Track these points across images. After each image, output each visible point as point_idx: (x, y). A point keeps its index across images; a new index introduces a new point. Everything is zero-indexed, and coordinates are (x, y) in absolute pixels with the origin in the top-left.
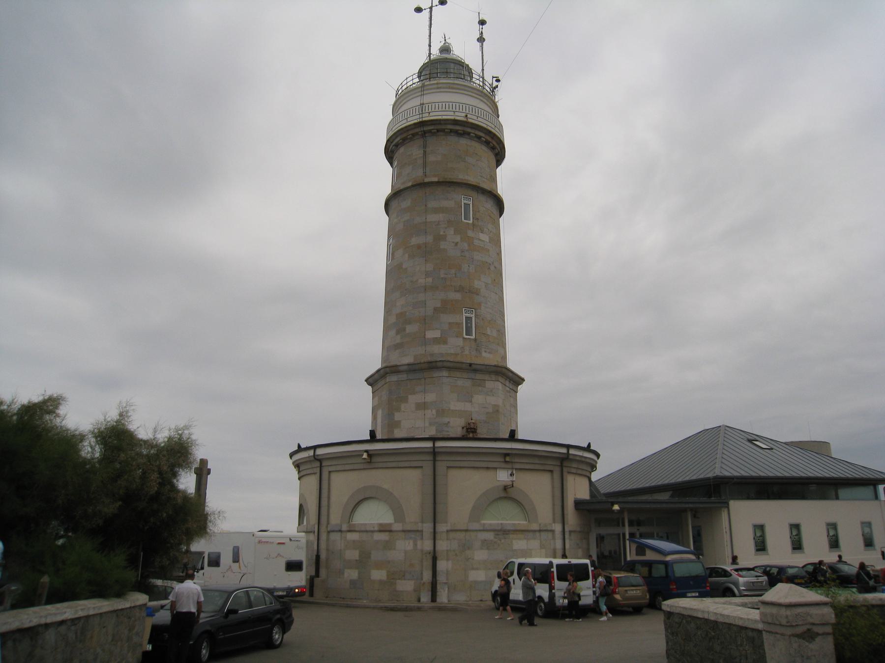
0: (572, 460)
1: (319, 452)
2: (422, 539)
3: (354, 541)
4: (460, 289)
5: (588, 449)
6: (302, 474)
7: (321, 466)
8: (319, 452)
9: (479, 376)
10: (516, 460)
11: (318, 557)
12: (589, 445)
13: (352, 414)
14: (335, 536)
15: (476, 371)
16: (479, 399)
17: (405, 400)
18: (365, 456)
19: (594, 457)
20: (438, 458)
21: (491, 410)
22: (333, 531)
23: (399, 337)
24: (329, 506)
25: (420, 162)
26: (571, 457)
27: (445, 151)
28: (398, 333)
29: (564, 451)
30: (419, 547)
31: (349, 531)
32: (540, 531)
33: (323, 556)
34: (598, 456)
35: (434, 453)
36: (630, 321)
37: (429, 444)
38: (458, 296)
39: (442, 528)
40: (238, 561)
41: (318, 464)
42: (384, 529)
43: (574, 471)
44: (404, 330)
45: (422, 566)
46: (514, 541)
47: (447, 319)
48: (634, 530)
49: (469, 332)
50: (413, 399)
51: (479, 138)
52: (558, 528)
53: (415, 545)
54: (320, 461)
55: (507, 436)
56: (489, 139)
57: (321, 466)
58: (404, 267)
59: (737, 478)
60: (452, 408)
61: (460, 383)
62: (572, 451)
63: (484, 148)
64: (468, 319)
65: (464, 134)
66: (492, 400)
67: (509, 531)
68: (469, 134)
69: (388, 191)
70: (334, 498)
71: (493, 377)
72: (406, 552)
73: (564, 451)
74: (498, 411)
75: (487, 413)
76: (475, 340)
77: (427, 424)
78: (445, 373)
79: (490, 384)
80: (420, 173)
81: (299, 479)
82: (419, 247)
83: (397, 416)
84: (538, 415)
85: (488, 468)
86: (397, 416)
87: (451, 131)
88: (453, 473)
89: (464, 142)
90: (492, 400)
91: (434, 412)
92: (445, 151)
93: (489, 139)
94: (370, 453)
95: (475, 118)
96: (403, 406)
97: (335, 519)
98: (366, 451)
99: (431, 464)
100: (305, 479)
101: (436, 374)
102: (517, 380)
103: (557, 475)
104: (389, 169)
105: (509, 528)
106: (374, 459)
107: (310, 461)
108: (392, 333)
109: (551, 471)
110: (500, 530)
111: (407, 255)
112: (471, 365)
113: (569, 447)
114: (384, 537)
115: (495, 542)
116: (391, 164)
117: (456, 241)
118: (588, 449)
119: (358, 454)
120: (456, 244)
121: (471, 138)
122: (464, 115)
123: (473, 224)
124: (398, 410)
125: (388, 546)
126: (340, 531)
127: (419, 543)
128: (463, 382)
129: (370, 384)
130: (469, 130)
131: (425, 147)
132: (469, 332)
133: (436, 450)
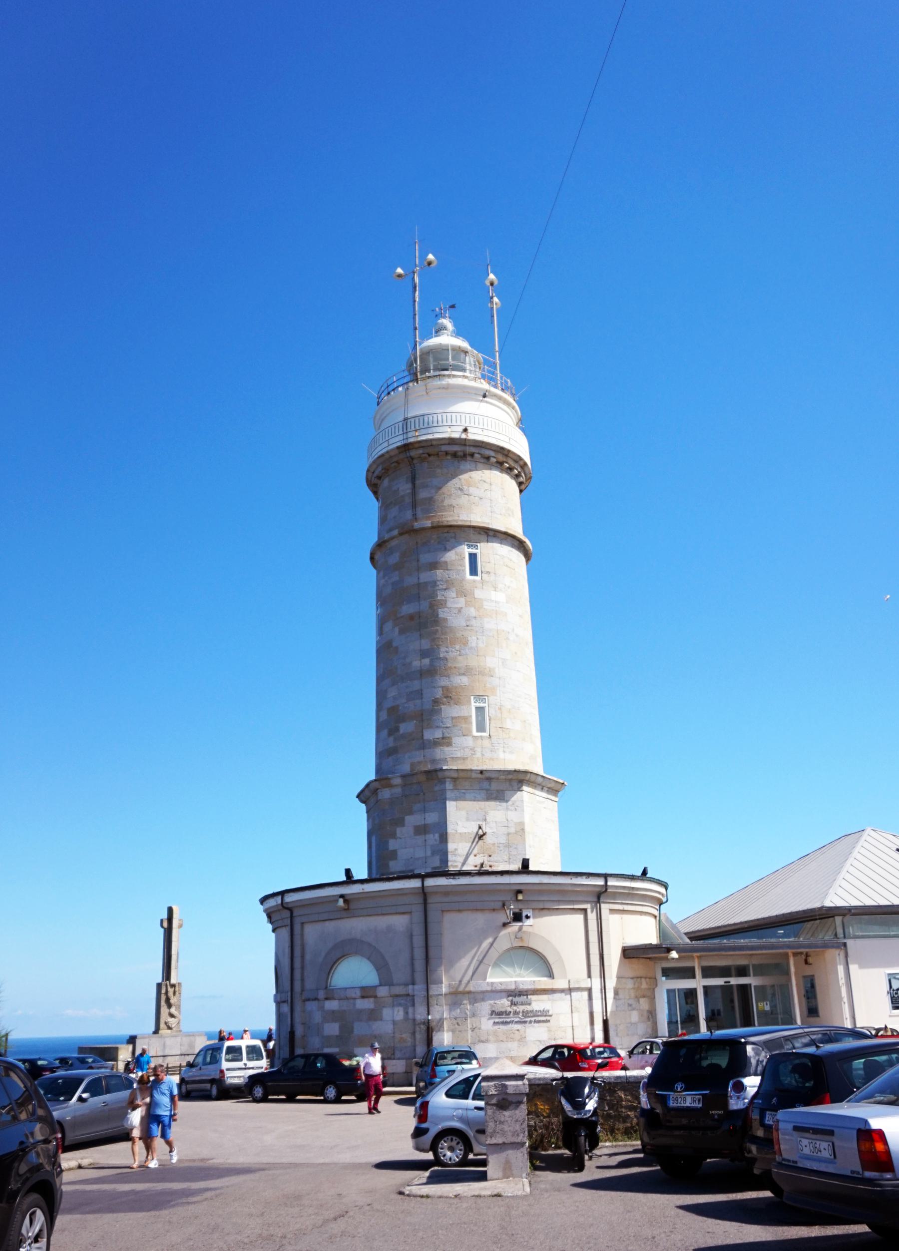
1: (289, 898)
2: (413, 1005)
3: (333, 1012)
6: (276, 924)
7: (292, 917)
8: (289, 898)
11: (292, 1034)
14: (312, 1006)
17: (401, 822)
18: (341, 901)
20: (429, 901)
21: (512, 830)
22: (309, 1000)
23: (391, 739)
24: (303, 968)
25: (408, 500)
28: (390, 734)
29: (600, 882)
30: (411, 1016)
31: (326, 999)
33: (299, 1032)
35: (424, 893)
37: (415, 883)
41: (287, 914)
42: (367, 992)
44: (397, 729)
45: (415, 1039)
50: (412, 820)
53: (407, 1013)
54: (291, 910)
55: (639, 873)
56: (501, 458)
57: (292, 917)
58: (394, 644)
59: (856, 907)
67: (483, 992)
69: (374, 539)
70: (308, 957)
72: (394, 1023)
73: (600, 882)
75: (508, 834)
77: (429, 853)
80: (409, 514)
81: (274, 931)
82: (411, 617)
83: (392, 844)
86: (392, 844)
91: (437, 836)
93: (501, 458)
94: (347, 898)
95: (479, 431)
96: (399, 831)
97: (310, 984)
98: (342, 896)
99: (421, 908)
100: (277, 930)
105: (526, 987)
107: (279, 910)
108: (385, 732)
109: (303, 923)
111: (397, 630)
113: (606, 876)
114: (366, 1004)
116: (377, 499)
119: (334, 899)
122: (461, 429)
124: (393, 835)
125: (373, 1015)
126: (316, 999)
127: (410, 1010)
129: (362, 801)
131: (413, 480)
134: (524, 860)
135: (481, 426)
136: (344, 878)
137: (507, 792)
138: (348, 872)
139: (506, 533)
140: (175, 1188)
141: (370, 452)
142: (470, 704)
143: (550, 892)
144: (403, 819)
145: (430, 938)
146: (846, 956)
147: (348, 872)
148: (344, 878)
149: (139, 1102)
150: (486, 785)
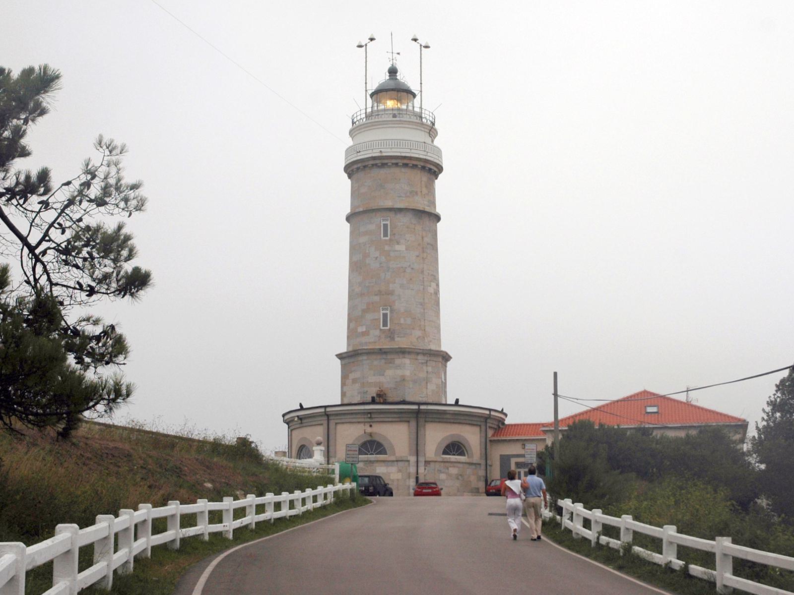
0: (421, 412)
1: (328, 409)
4: (379, 293)
5: (502, 412)
9: (389, 357)
10: (459, 418)
12: (502, 410)
13: (326, 389)
15: (386, 353)
16: (390, 373)
19: (503, 416)
20: (330, 418)
26: (492, 417)
27: (393, 183)
29: (488, 412)
32: (397, 461)
34: (506, 415)
36: (551, 314)
38: (376, 298)
39: (421, 459)
40: (524, 455)
43: (431, 420)
46: (377, 468)
47: (369, 316)
48: (65, 508)
49: (385, 324)
51: (397, 164)
52: (413, 459)
54: (328, 416)
60: (370, 381)
61: (376, 363)
62: (493, 413)
63: (403, 170)
64: (385, 315)
65: (384, 165)
66: (399, 372)
68: (386, 164)
71: (401, 356)
73: (488, 412)
74: (404, 379)
75: (396, 382)
76: (389, 330)
78: (365, 357)
79: (398, 361)
84: (464, 386)
85: (359, 422)
87: (373, 165)
88: (339, 427)
89: (383, 172)
90: (399, 372)
92: (393, 183)
98: (298, 416)
99: (326, 422)
101: (360, 358)
102: (446, 358)
103: (483, 428)
104: (349, 225)
106: (303, 421)
109: (480, 426)
110: (367, 461)
112: (380, 349)
113: (490, 410)
115: (364, 469)
117: (376, 256)
118: (502, 412)
120: (376, 258)
121: (389, 167)
123: (390, 240)
128: (377, 362)
130: (386, 161)
132: (385, 324)
133: (327, 413)
134: (372, 397)
135: (409, 147)
136: (299, 408)
137: (396, 360)
138: (301, 405)
139: (406, 209)
140: (209, 567)
141: (345, 163)
142: (380, 312)
143: (314, 417)
144: (348, 376)
145: (416, 437)
146: (417, 478)
147: (301, 405)
148: (299, 408)
149: (780, 419)
150: (384, 356)
